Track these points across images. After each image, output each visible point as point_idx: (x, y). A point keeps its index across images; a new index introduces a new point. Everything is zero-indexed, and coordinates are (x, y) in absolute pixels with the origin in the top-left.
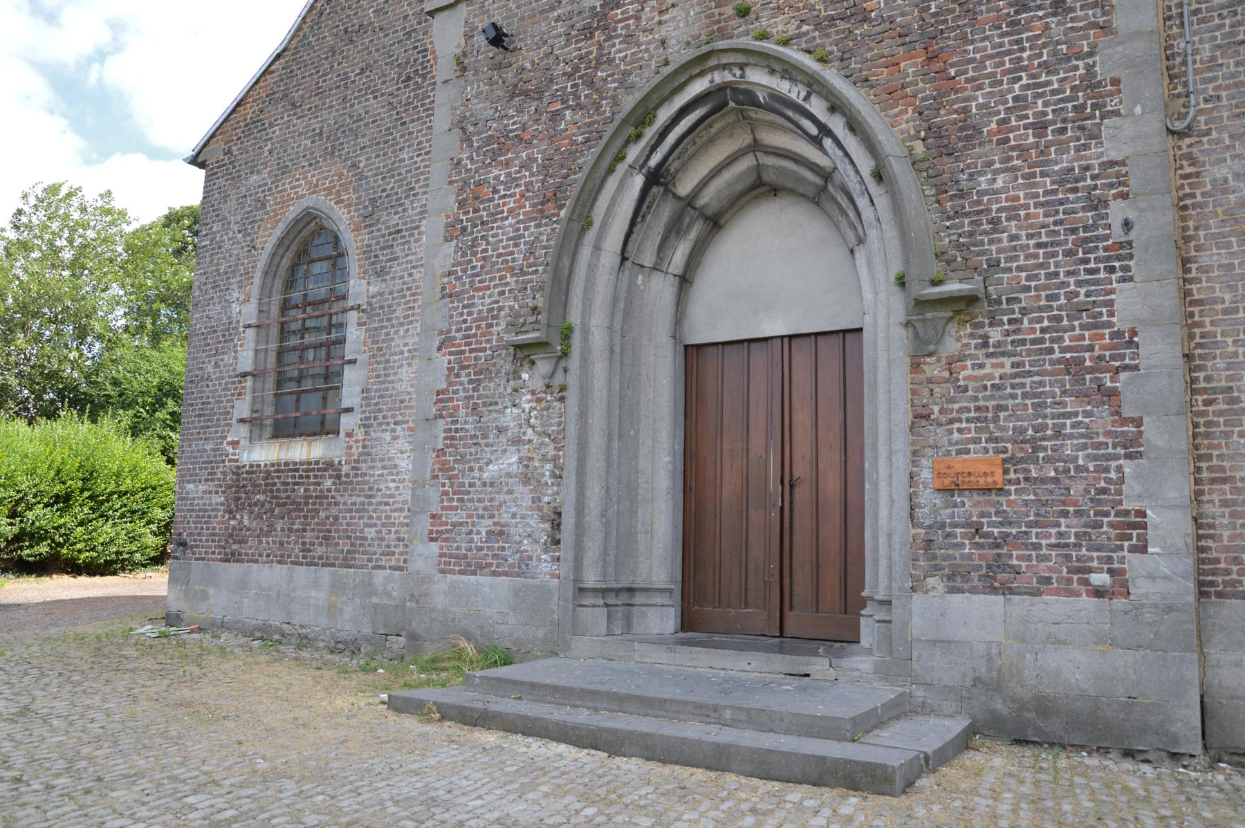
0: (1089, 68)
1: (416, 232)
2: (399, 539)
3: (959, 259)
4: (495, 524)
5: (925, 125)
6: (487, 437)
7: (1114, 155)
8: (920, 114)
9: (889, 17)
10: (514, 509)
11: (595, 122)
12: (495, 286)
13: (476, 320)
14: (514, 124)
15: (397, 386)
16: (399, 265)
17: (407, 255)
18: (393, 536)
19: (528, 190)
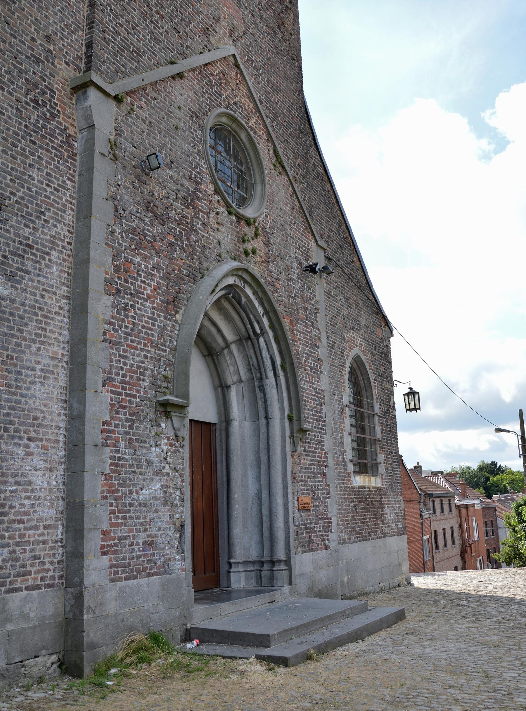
1: (47, 258)
2: (35, 558)
4: (148, 536)
6: (141, 468)
10: (159, 524)
15: (30, 402)
17: (39, 275)
18: (28, 555)
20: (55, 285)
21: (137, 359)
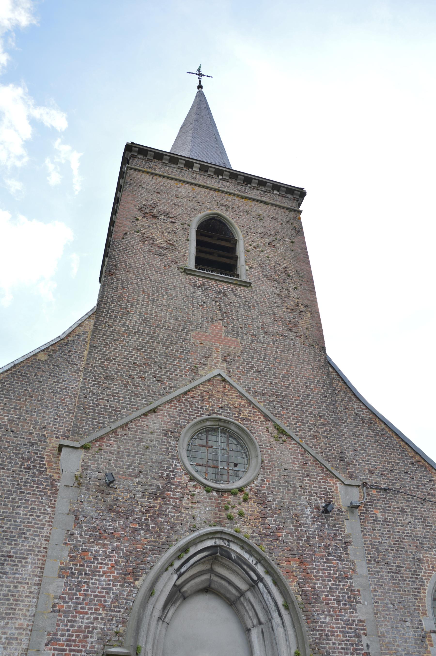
0: (351, 583)
1: (24, 561)
3: (317, 649)
5: (301, 589)
7: (361, 618)
8: (299, 584)
9: (287, 542)
11: (156, 542)
12: (91, 614)
13: (76, 631)
14: (109, 526)
16: (7, 578)
17: (14, 574)
19: (117, 565)
20: (28, 577)
21: (86, 621)
